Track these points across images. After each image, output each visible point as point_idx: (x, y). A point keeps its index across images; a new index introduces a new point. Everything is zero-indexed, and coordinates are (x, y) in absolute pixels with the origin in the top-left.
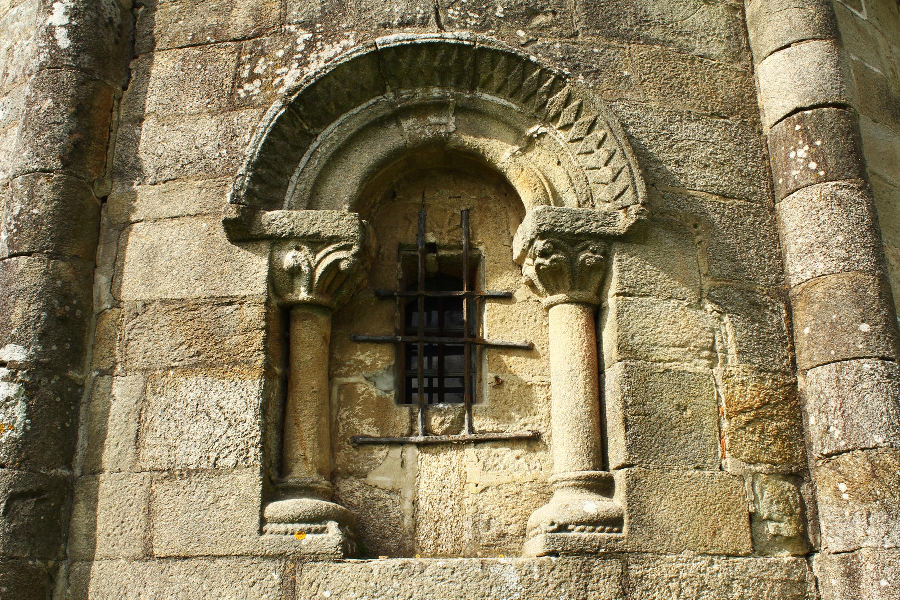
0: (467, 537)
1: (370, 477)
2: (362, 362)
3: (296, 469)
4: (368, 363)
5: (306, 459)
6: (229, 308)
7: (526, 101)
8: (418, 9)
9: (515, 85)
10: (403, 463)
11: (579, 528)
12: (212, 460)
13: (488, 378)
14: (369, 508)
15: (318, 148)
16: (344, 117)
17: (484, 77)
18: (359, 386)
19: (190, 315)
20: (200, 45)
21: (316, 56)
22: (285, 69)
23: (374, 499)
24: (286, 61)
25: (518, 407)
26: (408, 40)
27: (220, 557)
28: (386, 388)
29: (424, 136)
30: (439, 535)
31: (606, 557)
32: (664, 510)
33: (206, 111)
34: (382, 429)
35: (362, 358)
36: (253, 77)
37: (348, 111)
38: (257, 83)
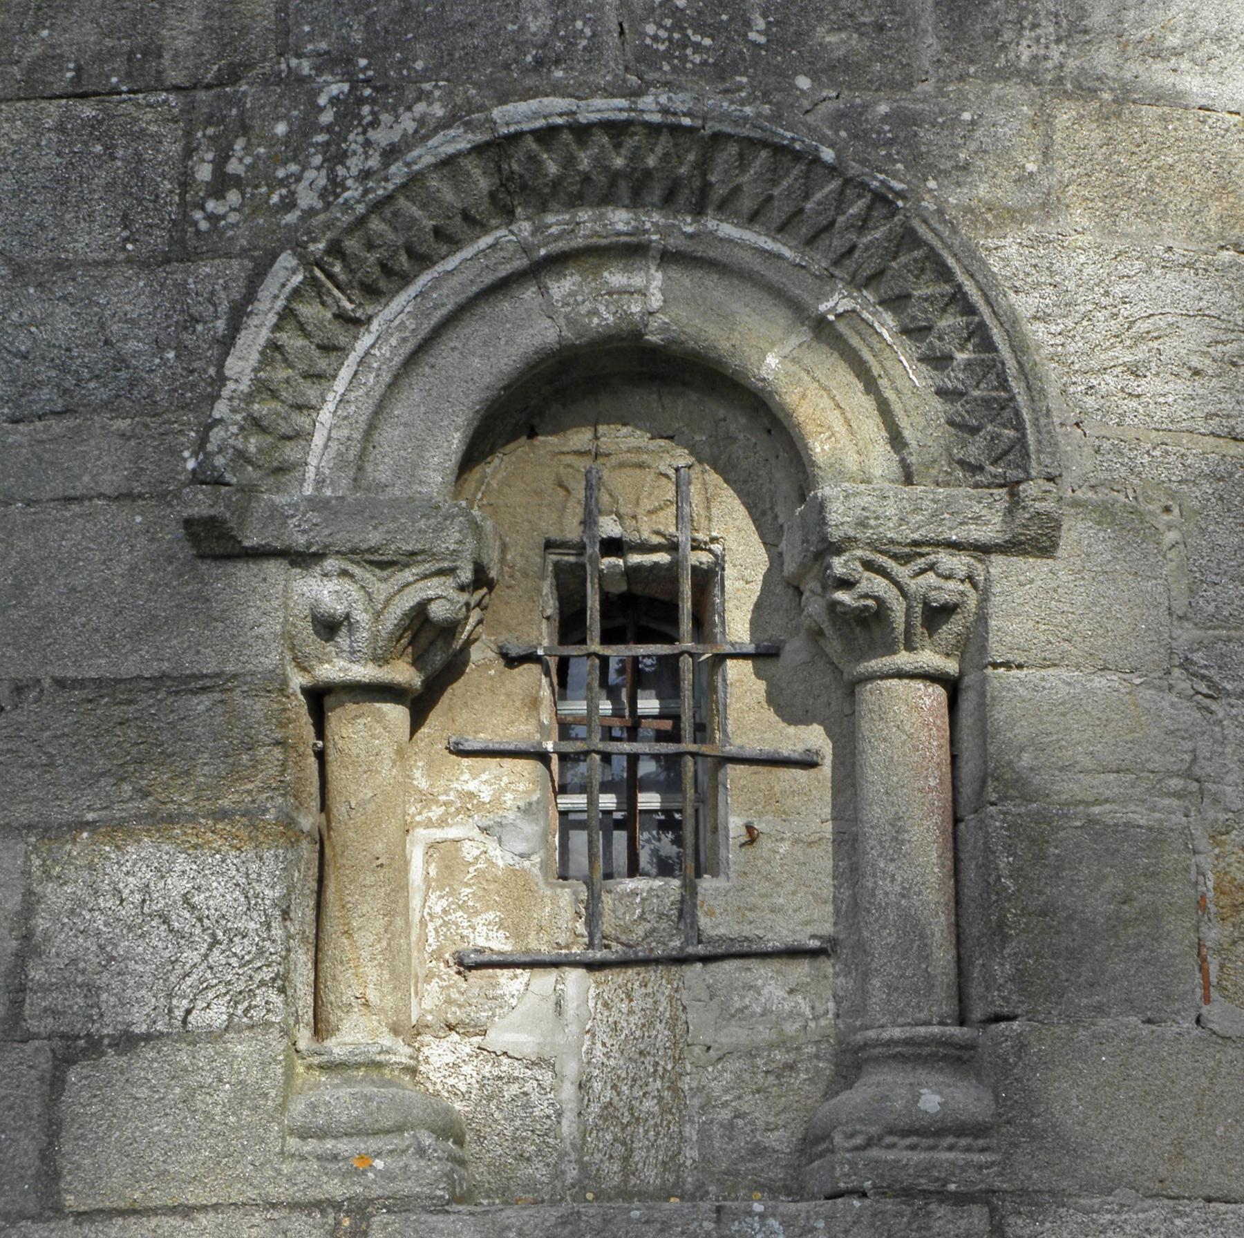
0: (691, 1154)
1: (491, 1034)
2: (471, 795)
3: (346, 1025)
4: (486, 796)
5: (366, 1004)
6: (204, 697)
7: (811, 241)
8: (579, 24)
9: (788, 209)
10: (558, 1004)
11: (908, 1141)
12: (179, 1013)
13: (731, 826)
14: (490, 1098)
15: (372, 346)
16: (425, 279)
17: (720, 191)
18: (467, 844)
19: (118, 712)
20: (96, 94)
21: (360, 139)
22: (293, 168)
23: (500, 1078)
24: (295, 148)
25: (791, 887)
26: (560, 115)
27: (204, 1208)
28: (522, 847)
29: (596, 320)
30: (632, 1150)
31: (961, 1200)
32: (1069, 1098)
33: (121, 256)
34: (516, 933)
35: (472, 786)
36: (221, 184)
37: (434, 264)
38: (233, 197)
